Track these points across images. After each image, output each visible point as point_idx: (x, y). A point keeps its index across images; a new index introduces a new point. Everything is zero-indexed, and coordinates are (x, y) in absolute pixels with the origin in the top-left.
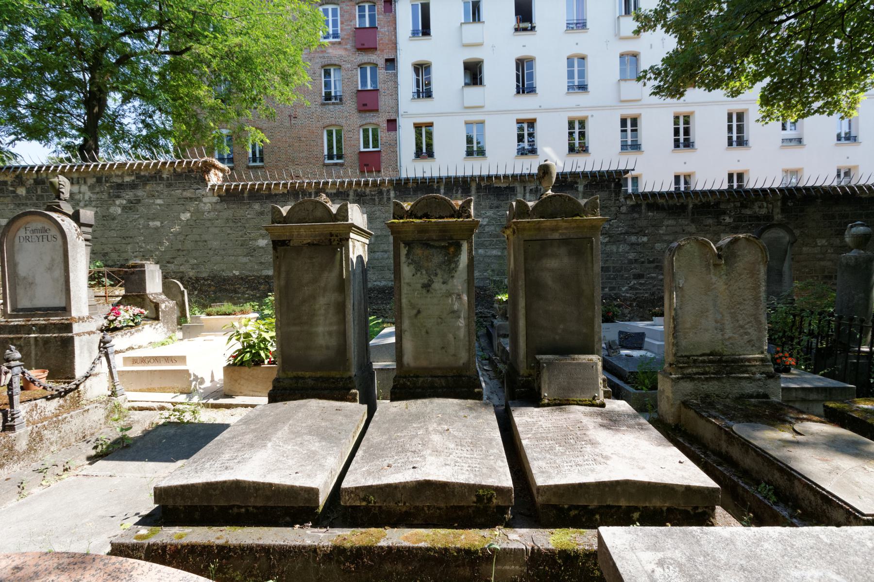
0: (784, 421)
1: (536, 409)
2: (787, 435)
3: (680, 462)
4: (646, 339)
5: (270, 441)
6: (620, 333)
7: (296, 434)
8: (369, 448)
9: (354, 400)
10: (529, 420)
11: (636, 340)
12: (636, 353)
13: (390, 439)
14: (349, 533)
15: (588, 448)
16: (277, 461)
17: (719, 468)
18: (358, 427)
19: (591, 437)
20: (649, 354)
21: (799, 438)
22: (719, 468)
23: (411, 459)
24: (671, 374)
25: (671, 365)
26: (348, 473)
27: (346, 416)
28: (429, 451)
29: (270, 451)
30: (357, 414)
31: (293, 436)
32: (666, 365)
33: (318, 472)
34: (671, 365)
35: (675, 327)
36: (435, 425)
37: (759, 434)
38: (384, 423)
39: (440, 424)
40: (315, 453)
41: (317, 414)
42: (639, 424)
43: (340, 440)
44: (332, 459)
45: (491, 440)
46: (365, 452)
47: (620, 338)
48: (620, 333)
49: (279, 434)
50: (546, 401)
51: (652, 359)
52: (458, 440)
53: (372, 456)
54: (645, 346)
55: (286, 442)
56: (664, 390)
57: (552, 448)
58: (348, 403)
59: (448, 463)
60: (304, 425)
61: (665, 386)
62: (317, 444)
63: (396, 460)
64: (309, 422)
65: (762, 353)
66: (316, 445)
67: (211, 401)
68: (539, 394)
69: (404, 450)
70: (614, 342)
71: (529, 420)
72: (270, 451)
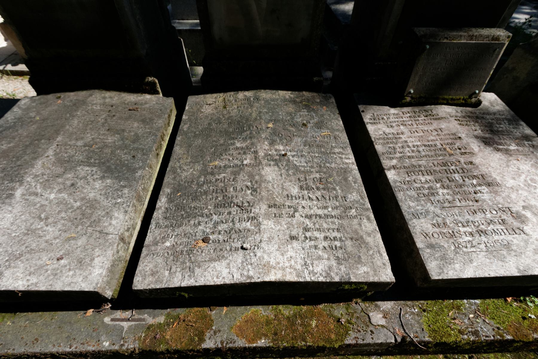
1: (393, 111)
5: (21, 182)
7: (66, 164)
8: (176, 190)
9: (156, 92)
10: (388, 130)
13: (204, 172)
14: (161, 319)
15: (485, 194)
16: (29, 232)
18: (160, 146)
19: (484, 170)
23: (237, 225)
26: (144, 251)
27: (144, 121)
28: (264, 207)
29: (18, 208)
30: (159, 117)
31: (59, 170)
33: (97, 252)
36: (266, 145)
38: (195, 136)
39: (272, 143)
40: (93, 204)
41: (101, 120)
43: (135, 170)
44: (121, 216)
45: (345, 171)
46: (170, 200)
49: (38, 167)
50: (408, 99)
52: (302, 177)
53: (182, 214)
55: (47, 185)
57: (432, 193)
58: (148, 96)
59: (294, 233)
60: (80, 143)
62: (98, 184)
63: (216, 224)
64: (89, 137)
66: (95, 187)
67: (9, 67)
69: (227, 203)
71: (388, 130)
72: (18, 208)
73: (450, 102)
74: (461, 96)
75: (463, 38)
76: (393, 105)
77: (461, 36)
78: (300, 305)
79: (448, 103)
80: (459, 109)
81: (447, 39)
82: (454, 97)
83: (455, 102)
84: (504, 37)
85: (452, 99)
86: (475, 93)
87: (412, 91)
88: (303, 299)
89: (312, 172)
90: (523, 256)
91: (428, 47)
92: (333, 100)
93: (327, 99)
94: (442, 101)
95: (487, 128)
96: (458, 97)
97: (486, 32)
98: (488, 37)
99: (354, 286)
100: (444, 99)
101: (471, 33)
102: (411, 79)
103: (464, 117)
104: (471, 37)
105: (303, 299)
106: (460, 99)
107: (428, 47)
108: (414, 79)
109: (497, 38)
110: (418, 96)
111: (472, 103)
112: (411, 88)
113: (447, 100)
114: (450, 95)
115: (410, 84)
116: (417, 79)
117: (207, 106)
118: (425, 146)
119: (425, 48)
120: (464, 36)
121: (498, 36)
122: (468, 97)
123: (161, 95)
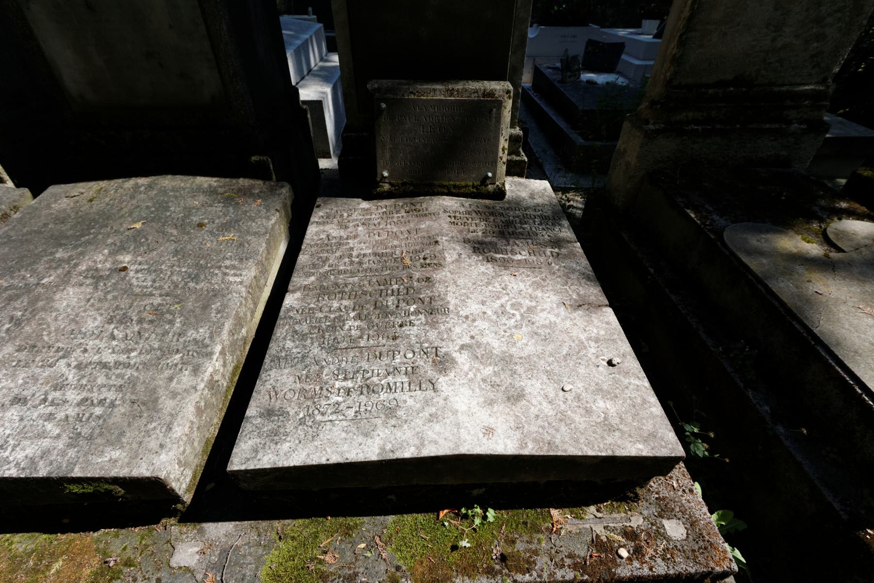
0: (810, 216)
2: (814, 249)
3: (610, 363)
4: (623, 57)
6: (590, 43)
11: (605, 57)
12: (601, 79)
17: (673, 297)
20: (621, 81)
21: (834, 255)
22: (673, 297)
24: (647, 123)
25: (653, 103)
32: (644, 105)
34: (653, 103)
35: (690, 19)
37: (754, 241)
42: (557, 243)
47: (586, 53)
48: (590, 43)
50: (386, 187)
51: (622, 88)
54: (619, 67)
56: (625, 151)
61: (630, 145)
65: (824, 81)
68: (373, 171)
70: (575, 58)
73: (453, 190)
74: (470, 181)
75: (438, 93)
76: (366, 198)
77: (434, 90)
78: (56, 533)
79: (450, 194)
80: (467, 202)
81: (414, 94)
82: (458, 183)
83: (462, 191)
84: (501, 93)
85: (455, 186)
86: (487, 177)
87: (386, 174)
88: (66, 521)
89: (154, 295)
90: (405, 427)
91: (384, 105)
92: (285, 191)
93: (272, 191)
94: (440, 190)
95: (497, 229)
96: (463, 183)
97: (474, 85)
98: (476, 91)
99: (90, 489)
100: (443, 186)
101: (450, 87)
102: (378, 156)
103: (469, 213)
104: (451, 92)
105: (66, 521)
106: (467, 186)
107: (384, 105)
108: (383, 156)
109: (491, 94)
110: (400, 182)
111: (489, 192)
112: (384, 169)
113: (447, 187)
114: (450, 180)
115: (380, 163)
116: (388, 156)
117: (351, 230)
118: (375, 254)
119: (381, 111)
120: (440, 90)
121: (492, 90)
122: (479, 183)
123: (10, 184)
